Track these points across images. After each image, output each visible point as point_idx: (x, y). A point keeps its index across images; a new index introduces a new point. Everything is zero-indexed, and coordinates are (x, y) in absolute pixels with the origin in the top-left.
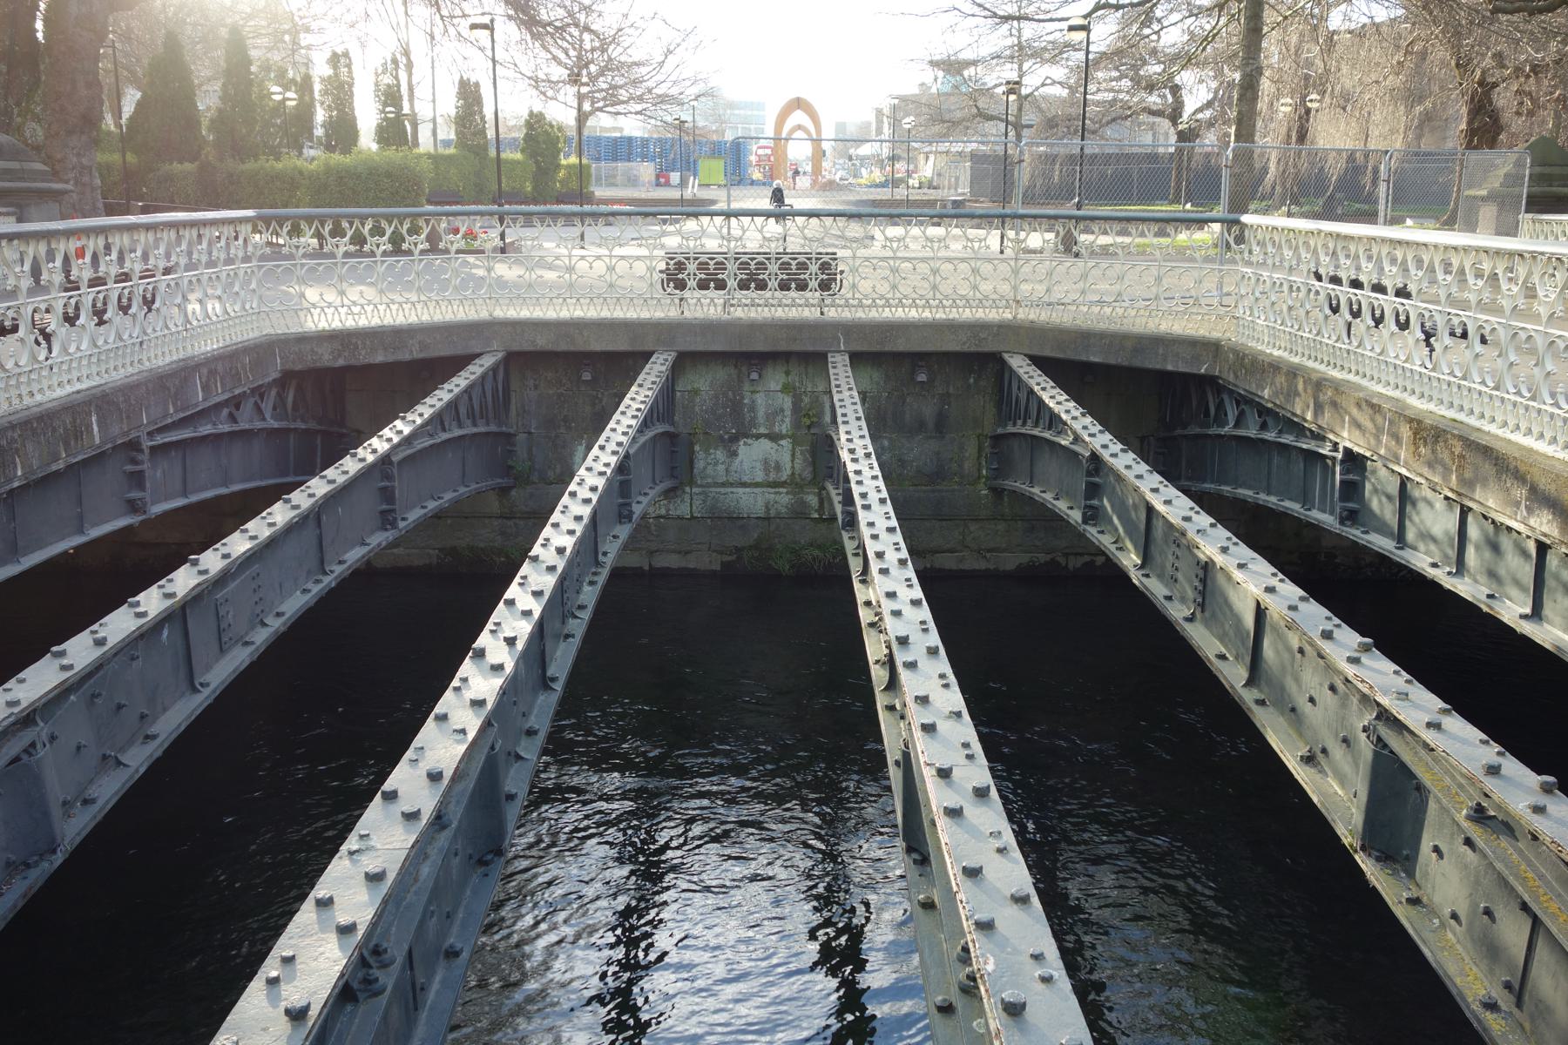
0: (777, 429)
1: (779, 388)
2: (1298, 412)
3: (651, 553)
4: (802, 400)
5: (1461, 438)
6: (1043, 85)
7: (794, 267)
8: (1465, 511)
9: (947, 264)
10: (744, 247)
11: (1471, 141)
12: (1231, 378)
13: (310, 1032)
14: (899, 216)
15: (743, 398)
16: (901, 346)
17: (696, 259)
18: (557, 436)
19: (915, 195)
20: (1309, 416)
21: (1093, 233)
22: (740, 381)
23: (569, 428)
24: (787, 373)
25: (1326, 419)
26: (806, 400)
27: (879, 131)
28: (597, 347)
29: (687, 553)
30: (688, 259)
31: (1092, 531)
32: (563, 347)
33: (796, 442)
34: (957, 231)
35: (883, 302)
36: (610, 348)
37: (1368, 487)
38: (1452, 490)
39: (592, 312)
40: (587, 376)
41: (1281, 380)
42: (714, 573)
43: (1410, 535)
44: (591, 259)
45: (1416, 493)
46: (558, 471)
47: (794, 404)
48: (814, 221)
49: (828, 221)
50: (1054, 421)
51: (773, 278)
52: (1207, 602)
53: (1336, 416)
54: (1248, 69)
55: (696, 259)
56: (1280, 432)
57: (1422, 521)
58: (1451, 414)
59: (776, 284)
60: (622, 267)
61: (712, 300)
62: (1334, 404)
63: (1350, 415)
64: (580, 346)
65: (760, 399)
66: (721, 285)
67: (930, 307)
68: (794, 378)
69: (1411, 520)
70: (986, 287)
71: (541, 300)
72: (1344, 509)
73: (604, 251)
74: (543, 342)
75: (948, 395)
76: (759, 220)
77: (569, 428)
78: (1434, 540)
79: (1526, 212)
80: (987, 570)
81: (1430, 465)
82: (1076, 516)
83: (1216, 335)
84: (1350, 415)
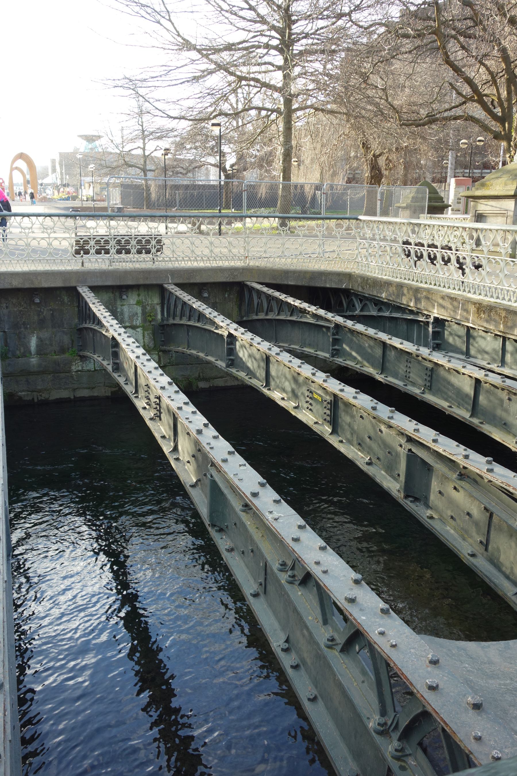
0: (134, 323)
1: (135, 303)
2: (405, 303)
3: (74, 390)
4: (146, 308)
5: (505, 309)
6: (156, 150)
7: (143, 242)
8: (504, 339)
9: (43, 241)
10: (119, 232)
11: (371, 181)
12: (360, 289)
13: (4, 652)
14: (139, 216)
15: (117, 309)
16: (198, 280)
17: (94, 239)
18: (20, 333)
19: (86, 204)
20: (412, 304)
21: (175, 223)
22: (115, 300)
23: (26, 328)
24: (139, 295)
25: (423, 305)
26: (148, 308)
27: (54, 170)
28: (45, 285)
29: (93, 388)
30: (90, 239)
31: (115, 375)
32: (27, 286)
33: (144, 329)
34: (122, 223)
35: (187, 258)
36: (53, 285)
37: (446, 332)
38: (500, 332)
39: (40, 267)
40: (37, 301)
41: (392, 289)
42: (107, 397)
43: (473, 352)
44: (60, 239)
45: (475, 334)
46: (22, 350)
47: (143, 310)
48: (26, 219)
49: (56, 219)
50: (201, 316)
51: (134, 247)
52: (433, 384)
53: (429, 303)
54: (287, 147)
55: (94, 239)
56: (391, 312)
57: (479, 346)
58: (492, 300)
59: (135, 251)
60: (56, 243)
61: (96, 260)
62: (427, 298)
63: (438, 302)
64: (37, 285)
65: (126, 309)
66: (107, 252)
67: (203, 261)
68: (142, 298)
69: (472, 345)
70: (217, 250)
71: (20, 261)
72: (434, 343)
73: (46, 235)
74: (16, 284)
75: (216, 303)
76: (41, 219)
77: (26, 328)
78: (487, 353)
79: (428, 213)
80: (238, 385)
81: (487, 321)
82: (110, 368)
83: (348, 270)
84: (438, 302)
